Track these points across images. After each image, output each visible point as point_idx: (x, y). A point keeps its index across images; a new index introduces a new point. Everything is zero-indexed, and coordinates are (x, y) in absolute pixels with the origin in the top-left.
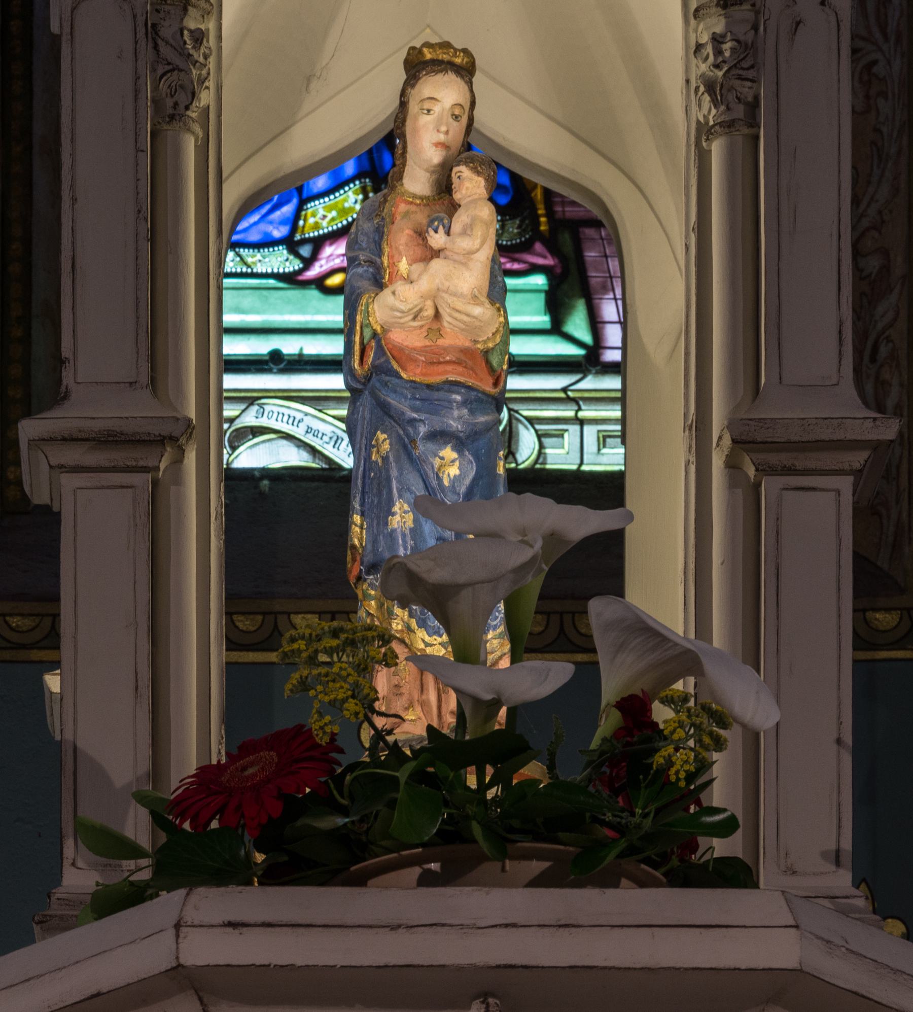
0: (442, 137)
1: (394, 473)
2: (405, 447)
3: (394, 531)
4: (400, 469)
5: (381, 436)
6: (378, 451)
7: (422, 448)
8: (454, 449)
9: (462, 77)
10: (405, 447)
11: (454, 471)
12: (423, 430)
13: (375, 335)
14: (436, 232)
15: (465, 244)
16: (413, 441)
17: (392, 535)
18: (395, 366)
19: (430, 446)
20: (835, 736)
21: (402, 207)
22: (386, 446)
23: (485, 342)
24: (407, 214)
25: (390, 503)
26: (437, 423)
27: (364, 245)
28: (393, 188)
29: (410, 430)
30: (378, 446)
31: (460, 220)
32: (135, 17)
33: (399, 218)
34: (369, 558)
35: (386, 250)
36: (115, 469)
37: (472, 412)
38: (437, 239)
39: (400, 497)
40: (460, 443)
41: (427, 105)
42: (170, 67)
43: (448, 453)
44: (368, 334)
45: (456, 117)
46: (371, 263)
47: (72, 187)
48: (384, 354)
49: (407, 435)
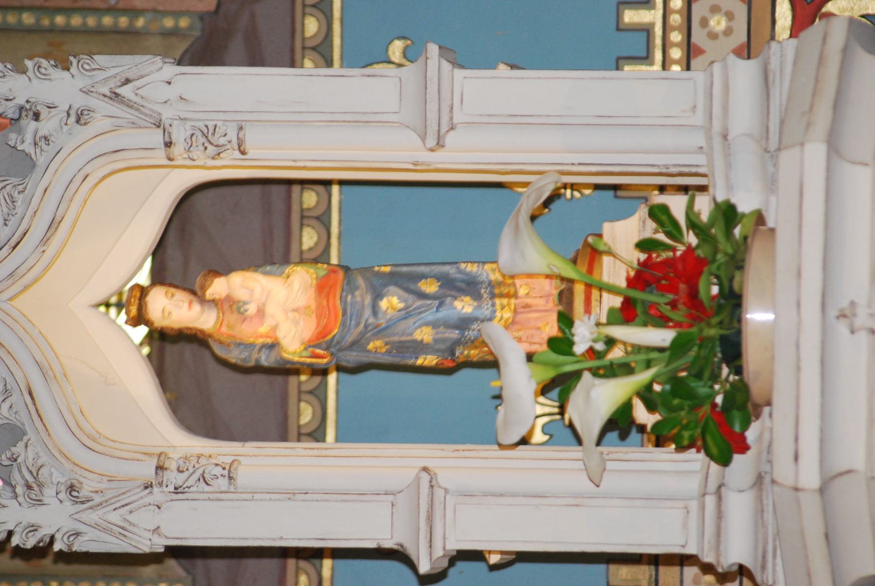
0: (186, 305)
1: (396, 338)
2: (380, 332)
3: (434, 339)
4: (394, 335)
5: (371, 346)
6: (381, 348)
7: (383, 322)
8: (381, 299)
9: (633, 346)
10: (379, 332)
11: (395, 300)
12: (371, 320)
13: (306, 349)
14: (246, 311)
15: (258, 291)
16: (378, 326)
17: (436, 341)
18: (329, 337)
19: (380, 315)
20: (131, 77)
21: (224, 329)
22: (378, 343)
23: (312, 279)
24: (230, 327)
25: (415, 341)
26: (368, 312)
27: (247, 354)
28: (210, 336)
29: (370, 328)
30: (377, 348)
31: (241, 294)
32: (172, 500)
33: (231, 332)
34: (446, 355)
35: (252, 340)
36: (343, 495)
37: (357, 288)
38: (252, 309)
39: (411, 334)
40: (378, 296)
41: (166, 314)
42: (202, 479)
43: (384, 304)
44: (305, 354)
45: (173, 295)
46: (260, 350)
47: (274, 539)
48: (320, 344)
49: (372, 330)
